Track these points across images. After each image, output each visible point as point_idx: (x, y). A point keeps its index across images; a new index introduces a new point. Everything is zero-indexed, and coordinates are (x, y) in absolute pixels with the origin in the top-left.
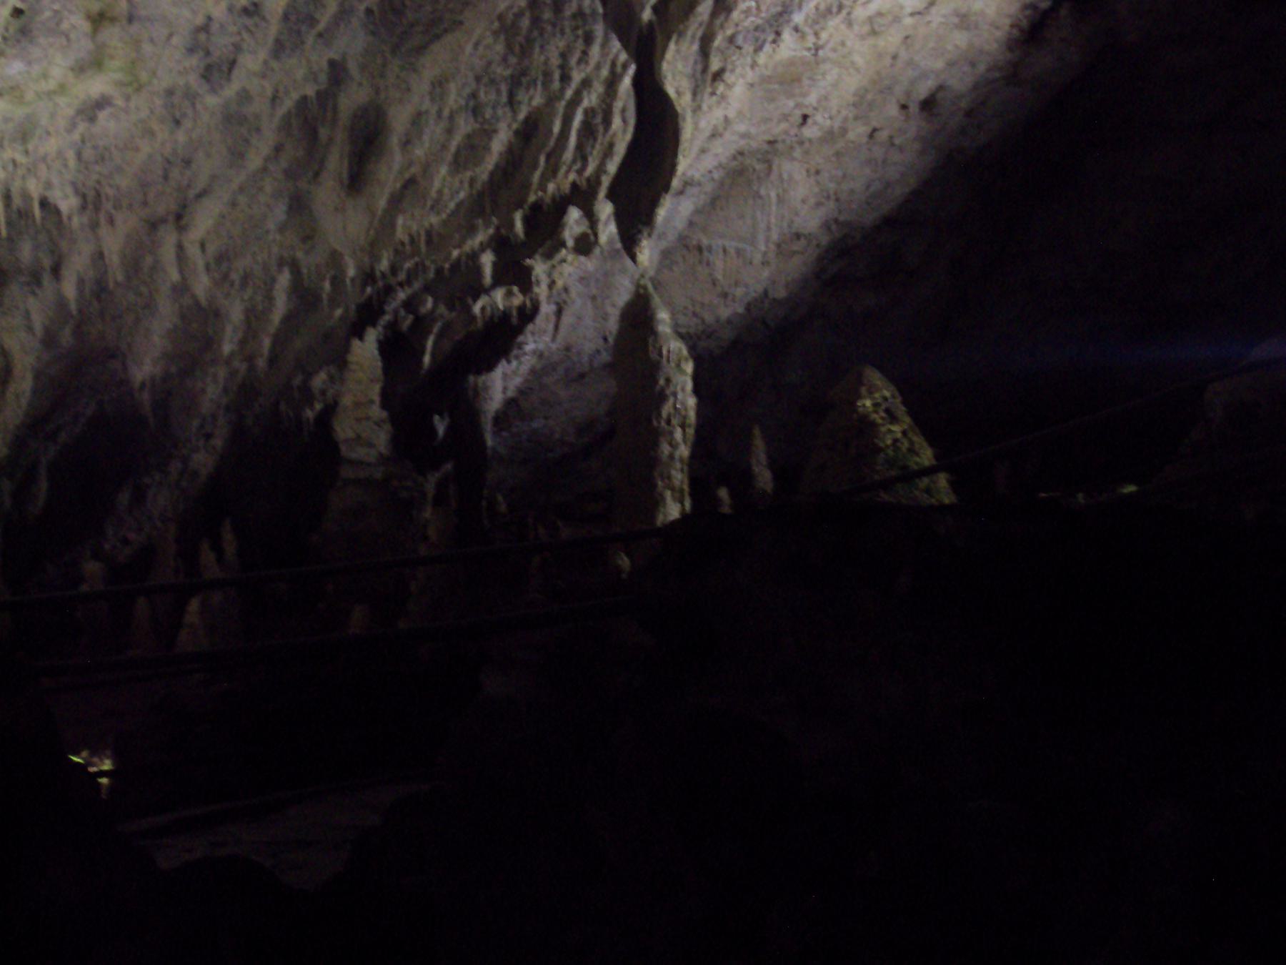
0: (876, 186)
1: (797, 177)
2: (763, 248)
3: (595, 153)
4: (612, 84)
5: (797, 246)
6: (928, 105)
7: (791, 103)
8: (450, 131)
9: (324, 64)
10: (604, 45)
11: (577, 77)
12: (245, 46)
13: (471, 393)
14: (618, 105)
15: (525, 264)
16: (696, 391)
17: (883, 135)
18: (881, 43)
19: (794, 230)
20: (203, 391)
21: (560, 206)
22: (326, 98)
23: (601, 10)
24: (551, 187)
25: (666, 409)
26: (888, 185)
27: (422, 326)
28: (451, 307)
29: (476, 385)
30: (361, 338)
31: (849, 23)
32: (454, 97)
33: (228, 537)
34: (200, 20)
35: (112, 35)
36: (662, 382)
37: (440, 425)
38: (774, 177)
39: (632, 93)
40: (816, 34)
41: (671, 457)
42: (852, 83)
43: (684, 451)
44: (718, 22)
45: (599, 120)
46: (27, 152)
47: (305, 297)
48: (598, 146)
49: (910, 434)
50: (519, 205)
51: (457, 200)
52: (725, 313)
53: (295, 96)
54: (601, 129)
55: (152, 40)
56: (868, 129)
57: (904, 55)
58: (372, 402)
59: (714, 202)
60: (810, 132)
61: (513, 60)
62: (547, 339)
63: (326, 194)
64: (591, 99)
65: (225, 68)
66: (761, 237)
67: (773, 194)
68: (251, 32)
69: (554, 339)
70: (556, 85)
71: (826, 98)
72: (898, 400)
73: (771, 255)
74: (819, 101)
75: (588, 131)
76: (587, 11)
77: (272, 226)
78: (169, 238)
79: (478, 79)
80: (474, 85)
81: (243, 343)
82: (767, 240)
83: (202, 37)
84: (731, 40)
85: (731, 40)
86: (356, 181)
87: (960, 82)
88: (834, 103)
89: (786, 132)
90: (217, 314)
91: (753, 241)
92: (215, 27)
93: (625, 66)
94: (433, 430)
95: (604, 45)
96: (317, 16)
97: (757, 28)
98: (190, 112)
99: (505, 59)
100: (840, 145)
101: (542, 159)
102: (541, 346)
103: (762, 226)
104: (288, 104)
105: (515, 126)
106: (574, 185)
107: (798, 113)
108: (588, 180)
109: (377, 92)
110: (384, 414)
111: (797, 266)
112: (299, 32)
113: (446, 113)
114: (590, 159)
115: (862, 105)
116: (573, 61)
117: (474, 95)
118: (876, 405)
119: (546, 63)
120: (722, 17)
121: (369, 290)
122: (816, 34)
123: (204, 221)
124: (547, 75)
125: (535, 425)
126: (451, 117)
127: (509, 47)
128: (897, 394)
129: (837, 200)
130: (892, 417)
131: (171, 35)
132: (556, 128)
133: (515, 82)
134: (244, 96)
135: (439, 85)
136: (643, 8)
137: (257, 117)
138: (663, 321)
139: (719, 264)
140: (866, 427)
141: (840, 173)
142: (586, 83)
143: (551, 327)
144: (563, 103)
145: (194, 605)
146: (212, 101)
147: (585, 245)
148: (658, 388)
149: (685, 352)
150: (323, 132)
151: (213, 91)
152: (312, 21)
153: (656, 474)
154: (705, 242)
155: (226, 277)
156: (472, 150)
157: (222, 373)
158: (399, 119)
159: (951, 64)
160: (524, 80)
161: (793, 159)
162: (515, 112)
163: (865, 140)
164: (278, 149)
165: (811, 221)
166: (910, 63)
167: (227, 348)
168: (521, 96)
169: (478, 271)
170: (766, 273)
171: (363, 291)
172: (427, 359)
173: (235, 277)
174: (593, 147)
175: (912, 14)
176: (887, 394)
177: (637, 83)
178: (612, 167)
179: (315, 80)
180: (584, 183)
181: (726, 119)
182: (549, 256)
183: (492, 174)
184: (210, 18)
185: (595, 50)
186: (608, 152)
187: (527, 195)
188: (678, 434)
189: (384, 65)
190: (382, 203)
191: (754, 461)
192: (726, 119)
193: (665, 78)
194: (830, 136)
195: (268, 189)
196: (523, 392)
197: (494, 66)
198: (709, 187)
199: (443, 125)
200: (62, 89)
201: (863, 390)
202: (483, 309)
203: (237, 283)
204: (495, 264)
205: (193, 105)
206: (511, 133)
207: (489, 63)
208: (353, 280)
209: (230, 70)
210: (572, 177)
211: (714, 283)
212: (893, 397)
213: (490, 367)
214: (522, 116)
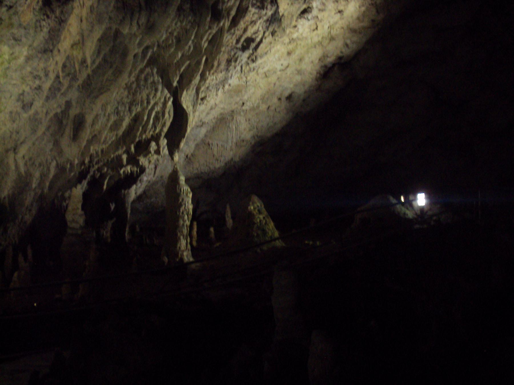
0: (271, 124)
1: (242, 121)
2: (230, 144)
3: (159, 126)
4: (165, 104)
5: (242, 144)
6: (289, 98)
7: (238, 99)
8: (108, 120)
9: (64, 102)
10: (162, 91)
11: (152, 102)
12: (36, 99)
13: (122, 196)
14: (167, 110)
15: (152, 142)
17: (272, 108)
18: (270, 79)
19: (241, 138)
20: (26, 199)
21: (148, 142)
22: (65, 112)
23: (161, 81)
24: (144, 137)
26: (275, 124)
27: (103, 176)
28: (113, 170)
29: (124, 195)
30: (76, 187)
31: (258, 74)
32: (110, 109)
33: (30, 252)
34: (21, 92)
36: (181, 200)
37: (113, 206)
38: (234, 121)
39: (172, 106)
40: (246, 78)
41: (183, 225)
42: (259, 93)
44: (202, 84)
45: (161, 115)
47: (61, 169)
48: (160, 123)
49: (266, 218)
50: (132, 142)
51: (112, 140)
52: (217, 166)
53: (54, 112)
54: (161, 118)
55: (5, 98)
56: (267, 107)
57: (278, 84)
58: (78, 209)
59: (214, 129)
60: (244, 108)
61: (130, 97)
62: (152, 176)
63: (65, 141)
64: (158, 108)
65: (29, 105)
66: (230, 142)
67: (234, 128)
68: (38, 95)
69: (154, 176)
71: (251, 97)
72: (263, 206)
73: (234, 147)
74: (248, 99)
75: (157, 118)
76: (156, 81)
77: (48, 150)
78: (11, 155)
79: (118, 103)
80: (117, 105)
81: (39, 184)
82: (232, 142)
83: (22, 97)
84: (208, 88)
85: (208, 88)
86: (75, 137)
87: (300, 91)
88: (253, 99)
89: (237, 108)
90: (31, 175)
91: (227, 142)
92: (26, 94)
93: (169, 98)
94: (110, 208)
95: (162, 91)
96: (61, 88)
97: (216, 84)
98: (18, 118)
99: (128, 97)
100: (257, 111)
101: (141, 128)
102: (149, 179)
103: (230, 138)
104: (51, 115)
105: (131, 118)
106: (152, 136)
107: (241, 102)
108: (157, 134)
109: (82, 109)
110: (83, 213)
111: (242, 151)
112: (55, 94)
113: (107, 114)
114: (157, 128)
115: (263, 99)
116: (151, 97)
117: (117, 108)
118: (255, 208)
119: (142, 97)
120: (203, 82)
121: (83, 167)
122: (246, 78)
123: (23, 151)
124: (142, 102)
125: (152, 200)
126: (109, 114)
127: (129, 93)
128: (262, 204)
129: (257, 129)
130: (260, 212)
131: (11, 97)
132: (145, 118)
133: (131, 104)
134: (36, 113)
135: (104, 107)
136: (174, 82)
137: (41, 119)
138: (182, 180)
139: (215, 149)
140: (251, 215)
141: (258, 120)
142: (156, 104)
143: (153, 173)
144: (148, 111)
145: (16, 274)
146: (25, 115)
147: (158, 152)
148: (179, 202)
149: (189, 190)
150: (64, 122)
151: (26, 112)
152: (59, 90)
153: (178, 231)
154: (210, 142)
155: (34, 163)
156: (116, 126)
157: (32, 194)
158: (89, 119)
159: (296, 85)
160: (134, 104)
161: (241, 116)
162: (131, 115)
163: (266, 110)
164: (49, 128)
165: (248, 135)
166: (280, 86)
167: (34, 186)
168: (134, 108)
169: (121, 160)
170: (231, 153)
171: (81, 166)
172: (105, 187)
173: (37, 163)
174: (158, 124)
175: (280, 71)
176: (259, 204)
177: (174, 103)
178: (165, 130)
179: (61, 107)
180: (155, 135)
181: (216, 104)
182: (145, 156)
183: (124, 133)
184: (24, 91)
185: (159, 94)
186: (164, 125)
187: (136, 138)
188: (186, 217)
189: (85, 101)
190: (84, 143)
191: (226, 216)
192: (216, 104)
193: (183, 103)
194: (253, 109)
195: (45, 139)
196: (144, 192)
197: (124, 99)
198: (212, 124)
199: (106, 117)
201: (251, 203)
202: (124, 172)
203: (37, 165)
204: (127, 158)
205: (19, 116)
206: (130, 120)
207: (122, 98)
208: (77, 164)
209: (31, 106)
210: (151, 133)
211: (214, 156)
212: (261, 206)
213: (130, 187)
214: (133, 114)
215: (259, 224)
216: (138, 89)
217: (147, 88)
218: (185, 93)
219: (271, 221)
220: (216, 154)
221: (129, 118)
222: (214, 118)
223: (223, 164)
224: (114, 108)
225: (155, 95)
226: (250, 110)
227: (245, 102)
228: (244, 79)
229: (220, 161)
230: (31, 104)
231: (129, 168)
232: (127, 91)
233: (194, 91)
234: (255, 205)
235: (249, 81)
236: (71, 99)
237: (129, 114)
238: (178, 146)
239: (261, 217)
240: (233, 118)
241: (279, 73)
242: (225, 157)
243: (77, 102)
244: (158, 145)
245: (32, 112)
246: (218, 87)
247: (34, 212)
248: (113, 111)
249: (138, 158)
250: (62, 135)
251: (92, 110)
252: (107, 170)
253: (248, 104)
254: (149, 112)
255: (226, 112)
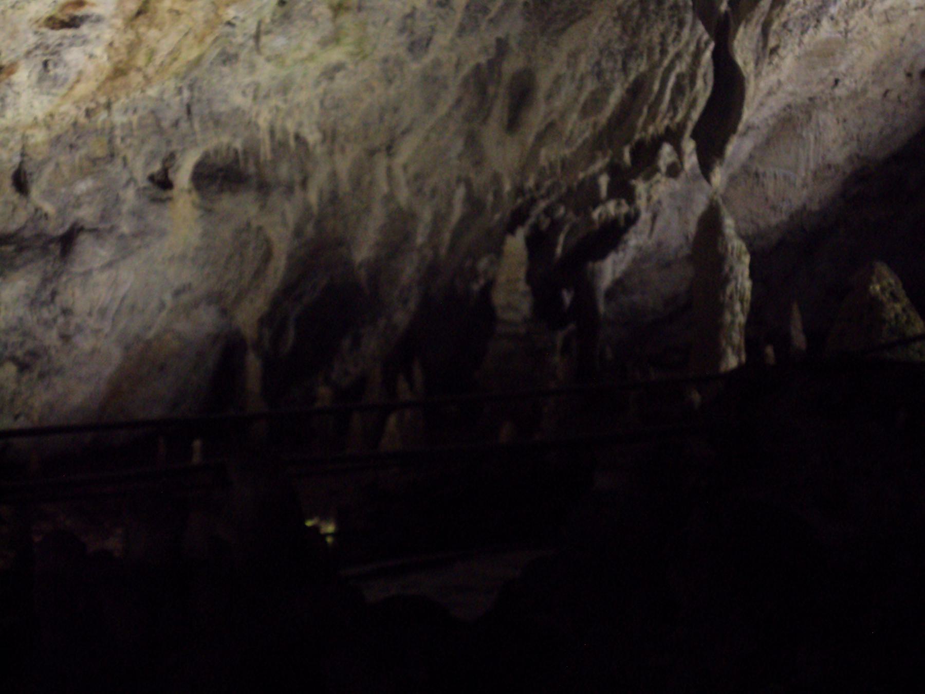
7: (826, 71)
8: (580, 89)
9: (494, 42)
10: (693, 28)
11: (672, 51)
14: (701, 72)
16: (752, 276)
17: (893, 95)
18: (893, 28)
22: (494, 64)
25: (730, 289)
27: (556, 225)
28: (577, 213)
31: (871, 15)
32: (584, 66)
34: (408, 10)
35: (347, 20)
37: (567, 297)
38: (813, 124)
40: (847, 22)
41: (733, 323)
42: (871, 57)
43: (741, 319)
44: (775, 12)
46: (285, 101)
47: (474, 204)
48: (686, 100)
50: (627, 142)
52: (774, 220)
53: (472, 64)
54: (688, 89)
56: (882, 91)
60: (840, 91)
63: (492, 132)
64: (681, 67)
66: (802, 166)
70: (657, 56)
72: (900, 285)
74: (847, 70)
75: (679, 90)
78: (382, 162)
79: (601, 52)
82: (806, 170)
84: (785, 25)
85: (785, 25)
86: (513, 124)
89: (823, 92)
92: (418, 14)
93: (707, 44)
95: (693, 28)
97: (803, 17)
99: (620, 39)
100: (862, 101)
101: (645, 110)
102: (641, 242)
104: (466, 69)
105: (626, 86)
106: (668, 129)
107: (831, 79)
108: (678, 124)
111: (828, 188)
115: (879, 73)
116: (670, 39)
117: (598, 63)
118: (883, 290)
122: (847, 22)
123: (406, 151)
124: (651, 50)
127: (624, 29)
129: (858, 140)
130: (894, 298)
131: (387, 21)
132: (656, 87)
134: (437, 64)
135: (574, 56)
140: (875, 304)
141: (861, 122)
142: (678, 56)
143: (647, 231)
145: (392, 420)
146: (415, 67)
147: (674, 171)
149: (744, 248)
150: (491, 90)
152: (485, 10)
154: (761, 170)
156: (595, 103)
157: (415, 257)
158: (544, 81)
163: (879, 98)
164: (459, 102)
165: (839, 155)
166: (914, 44)
167: (420, 240)
168: (632, 64)
169: (596, 187)
170: (805, 193)
172: (559, 250)
173: (427, 190)
175: (916, 9)
177: (715, 55)
178: (695, 115)
182: (648, 178)
183: (610, 120)
185: (686, 32)
186: (692, 105)
188: (738, 307)
190: (531, 139)
194: (854, 95)
198: (765, 131)
200: (311, 57)
201: (874, 278)
202: (600, 215)
207: (610, 41)
209: (428, 44)
210: (666, 122)
211: (767, 199)
212: (896, 283)
213: (603, 256)
214: (632, 77)
215: (893, 323)
216: (644, 20)
217: (663, 20)
218: (741, 30)
219: (919, 318)
220: (770, 193)
221: (622, 85)
222: (773, 116)
223: (784, 218)
224: (593, 61)
225: (678, 34)
226: (848, 98)
227: (840, 77)
228: (842, 25)
229: (781, 212)
230: (429, 40)
231: (611, 207)
232: (619, 23)
233: (758, 30)
234: (885, 283)
235: (851, 31)
236: (508, 35)
237: (623, 77)
238: (719, 152)
239: (898, 307)
240: (810, 118)
241: (913, 14)
242: (790, 201)
243: (520, 44)
244: (678, 150)
245: (427, 60)
246: (807, 23)
247: (412, 305)
248: (589, 68)
249: (633, 182)
250: (485, 121)
251: (552, 60)
252: (566, 214)
253: (847, 82)
254: (664, 73)
255: (799, 100)
